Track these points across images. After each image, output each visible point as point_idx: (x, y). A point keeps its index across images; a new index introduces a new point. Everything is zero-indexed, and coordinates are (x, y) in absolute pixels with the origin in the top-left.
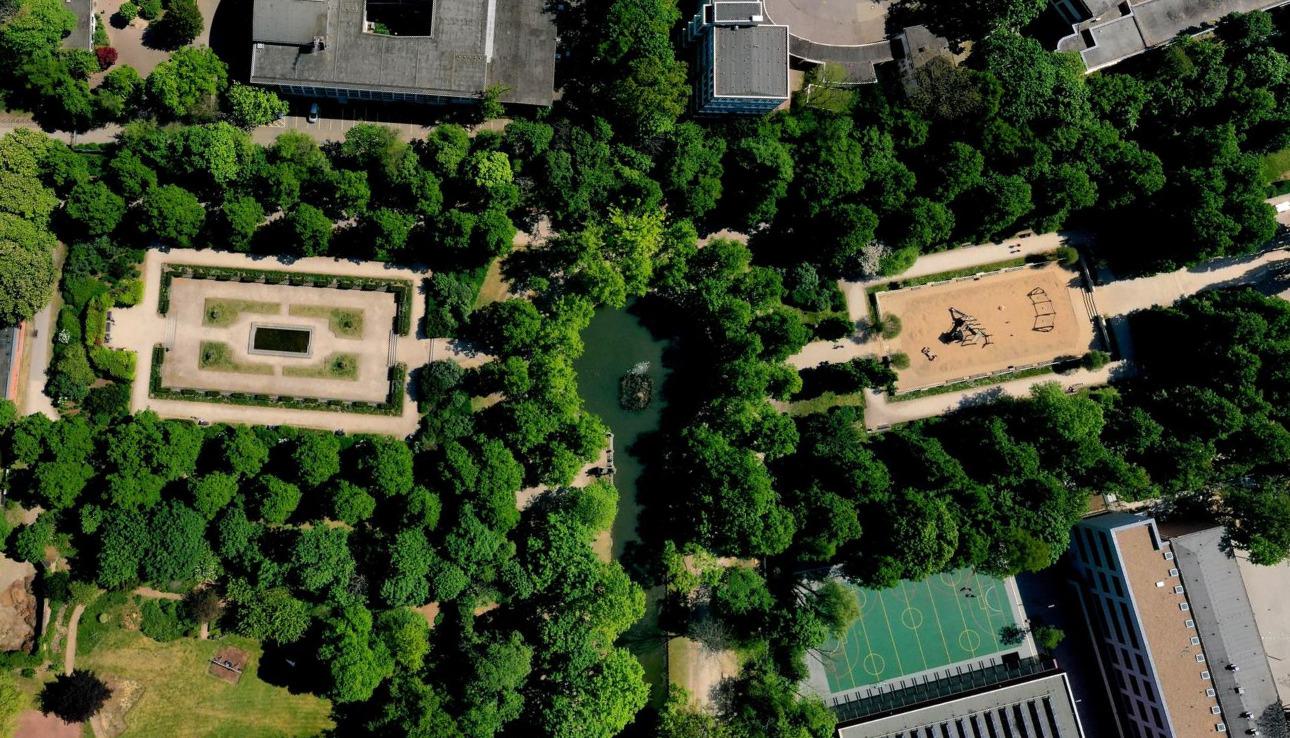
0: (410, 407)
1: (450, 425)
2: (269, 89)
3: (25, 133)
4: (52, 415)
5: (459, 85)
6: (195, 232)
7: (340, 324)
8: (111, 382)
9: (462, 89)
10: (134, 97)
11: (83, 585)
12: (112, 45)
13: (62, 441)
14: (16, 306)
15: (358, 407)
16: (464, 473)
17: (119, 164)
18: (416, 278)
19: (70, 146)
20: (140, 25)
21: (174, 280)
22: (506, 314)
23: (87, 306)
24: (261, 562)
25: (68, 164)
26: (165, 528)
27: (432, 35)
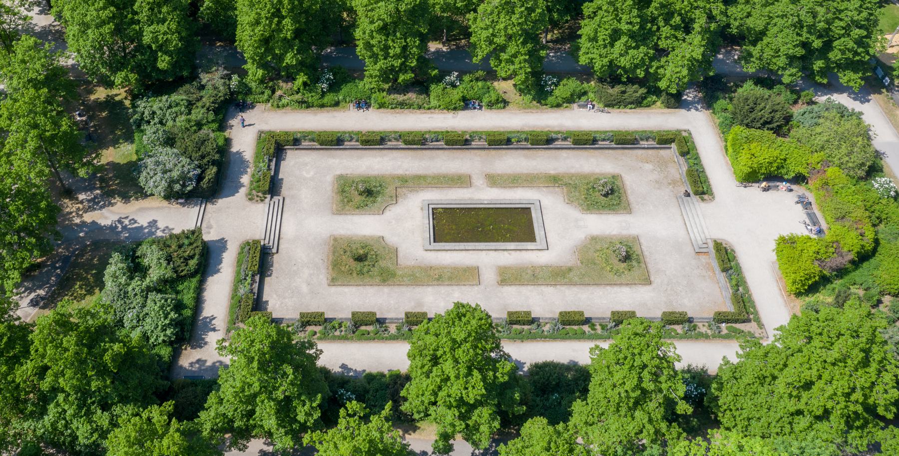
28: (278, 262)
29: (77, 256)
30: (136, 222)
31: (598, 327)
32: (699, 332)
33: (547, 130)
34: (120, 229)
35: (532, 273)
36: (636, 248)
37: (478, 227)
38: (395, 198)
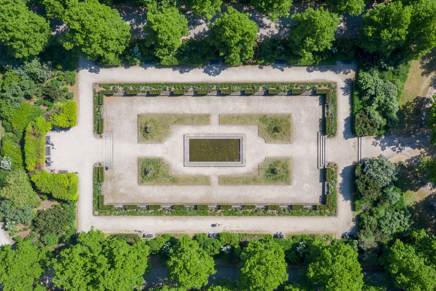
1: (387, 222)
6: (121, 49)
7: (269, 129)
8: (56, 203)
21: (106, 99)
28: (317, 128)
29: (417, 128)
30: (392, 149)
31: (168, 89)
32: (123, 87)
33: (173, 217)
34: (400, 145)
35: (194, 120)
36: (141, 135)
37: (217, 150)
38: (259, 168)
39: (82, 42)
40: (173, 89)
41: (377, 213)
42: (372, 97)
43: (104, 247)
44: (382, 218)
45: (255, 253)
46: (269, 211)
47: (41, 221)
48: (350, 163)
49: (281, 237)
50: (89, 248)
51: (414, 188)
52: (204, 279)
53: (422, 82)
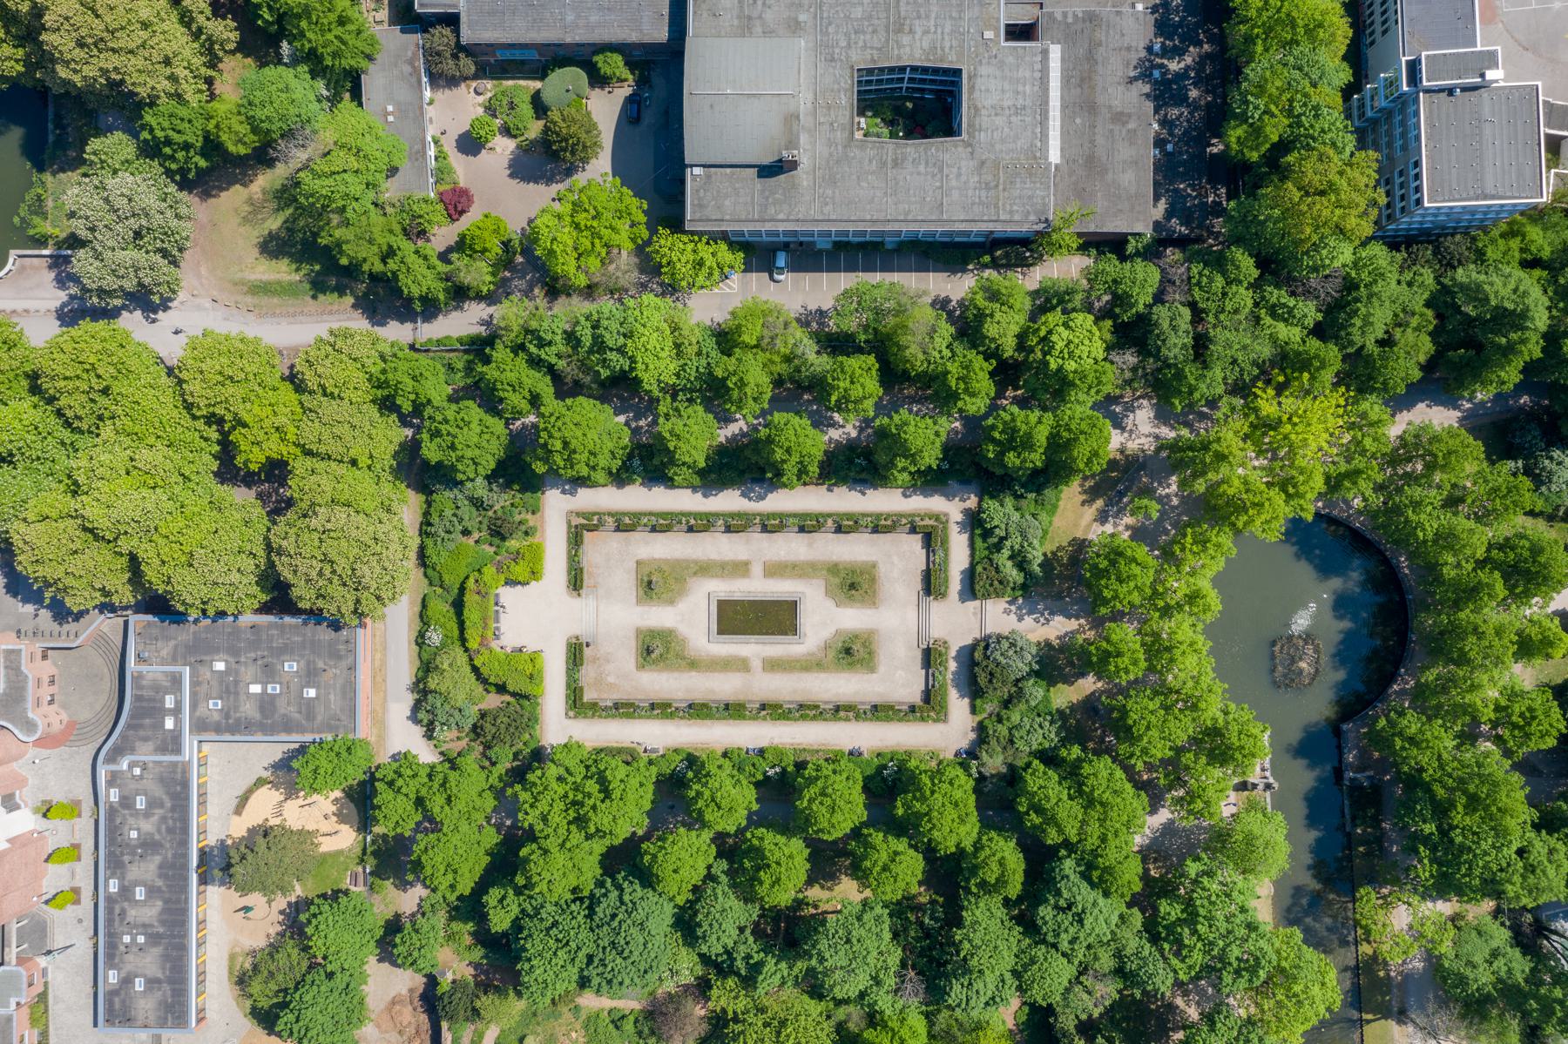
0: (958, 705)
1: (1023, 732)
2: (715, 237)
3: (347, 335)
4: (426, 755)
5: (1011, 212)
8: (508, 698)
9: (1017, 217)
10: (505, 262)
11: (497, 1002)
12: (462, 184)
13: (449, 800)
14: (358, 601)
15: (880, 712)
16: (1062, 814)
17: (496, 374)
18: (951, 508)
19: (412, 347)
20: (504, 147)
22: (1104, 564)
23: (462, 589)
24: (761, 964)
25: (414, 378)
26: (615, 924)
27: (964, 136)
28: (917, 584)
36: (641, 592)
38: (827, 647)
39: (562, 464)
40: (692, 522)
41: (1008, 719)
42: (1002, 539)
43: (587, 768)
44: (1017, 727)
45: (817, 778)
46: (842, 714)
47: (488, 726)
48: (969, 641)
49: (860, 754)
50: (567, 770)
51: (1068, 681)
52: (740, 817)
53: (1081, 516)
